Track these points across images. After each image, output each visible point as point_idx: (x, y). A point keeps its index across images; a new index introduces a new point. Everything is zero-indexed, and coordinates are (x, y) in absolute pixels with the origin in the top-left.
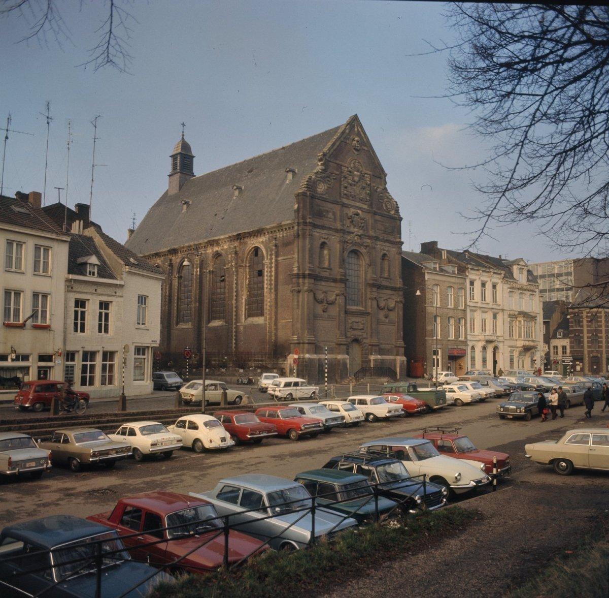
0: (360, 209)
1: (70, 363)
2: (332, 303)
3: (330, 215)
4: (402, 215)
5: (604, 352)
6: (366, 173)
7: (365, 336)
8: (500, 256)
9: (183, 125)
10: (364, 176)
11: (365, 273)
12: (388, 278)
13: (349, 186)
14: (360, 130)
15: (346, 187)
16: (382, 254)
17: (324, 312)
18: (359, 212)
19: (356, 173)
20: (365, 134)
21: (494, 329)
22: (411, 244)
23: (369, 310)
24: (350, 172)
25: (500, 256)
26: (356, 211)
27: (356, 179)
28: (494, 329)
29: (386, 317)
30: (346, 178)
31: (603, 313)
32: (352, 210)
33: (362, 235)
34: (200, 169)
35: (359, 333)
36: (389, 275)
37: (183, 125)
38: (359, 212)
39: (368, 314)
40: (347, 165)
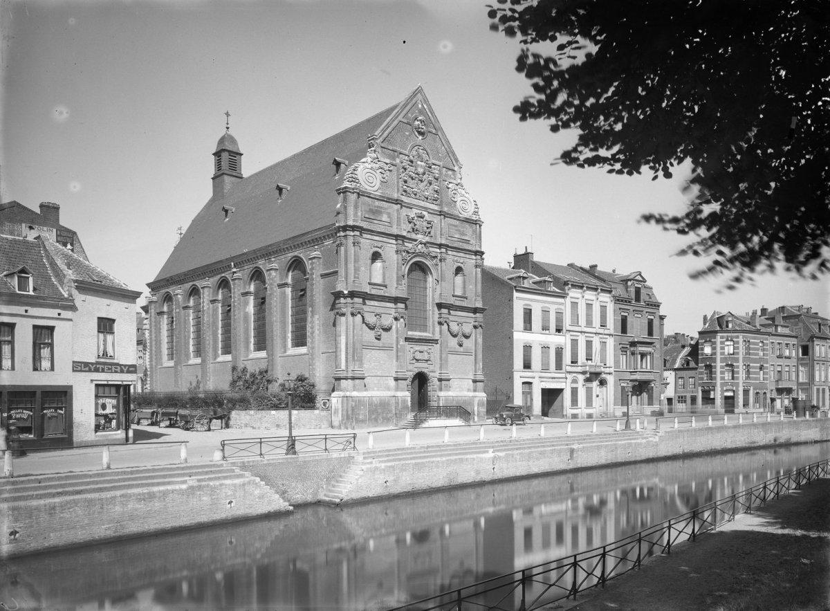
0: (426, 209)
1: (84, 408)
2: (387, 330)
3: (385, 218)
4: (624, 271)
5: (741, 385)
6: (434, 164)
7: (431, 368)
8: (614, 271)
9: (227, 114)
10: (430, 167)
11: (433, 291)
12: (464, 297)
13: (410, 180)
14: (425, 107)
15: (406, 182)
16: (455, 267)
17: (376, 338)
18: (425, 213)
19: (419, 163)
20: (432, 113)
21: (105, 341)
22: (498, 258)
23: (437, 336)
24: (412, 162)
25: (614, 271)
26: (420, 212)
27: (421, 170)
28: (105, 341)
29: (461, 345)
30: (405, 169)
31: (741, 337)
32: (415, 211)
33: (428, 243)
34: (249, 167)
35: (425, 365)
36: (465, 292)
37: (227, 114)
38: (425, 213)
39: (436, 341)
40: (407, 152)
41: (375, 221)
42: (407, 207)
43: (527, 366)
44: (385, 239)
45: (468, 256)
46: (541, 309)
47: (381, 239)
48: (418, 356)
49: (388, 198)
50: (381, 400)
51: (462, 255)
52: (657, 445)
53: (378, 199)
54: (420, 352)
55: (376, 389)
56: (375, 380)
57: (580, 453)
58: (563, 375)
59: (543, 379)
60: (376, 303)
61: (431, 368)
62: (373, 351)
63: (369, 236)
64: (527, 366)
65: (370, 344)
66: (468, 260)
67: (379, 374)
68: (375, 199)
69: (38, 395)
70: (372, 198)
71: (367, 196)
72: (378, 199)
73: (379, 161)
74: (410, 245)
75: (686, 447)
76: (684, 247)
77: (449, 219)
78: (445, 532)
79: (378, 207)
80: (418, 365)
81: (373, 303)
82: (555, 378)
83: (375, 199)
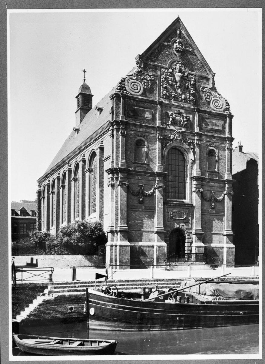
9: (85, 71)
37: (85, 71)
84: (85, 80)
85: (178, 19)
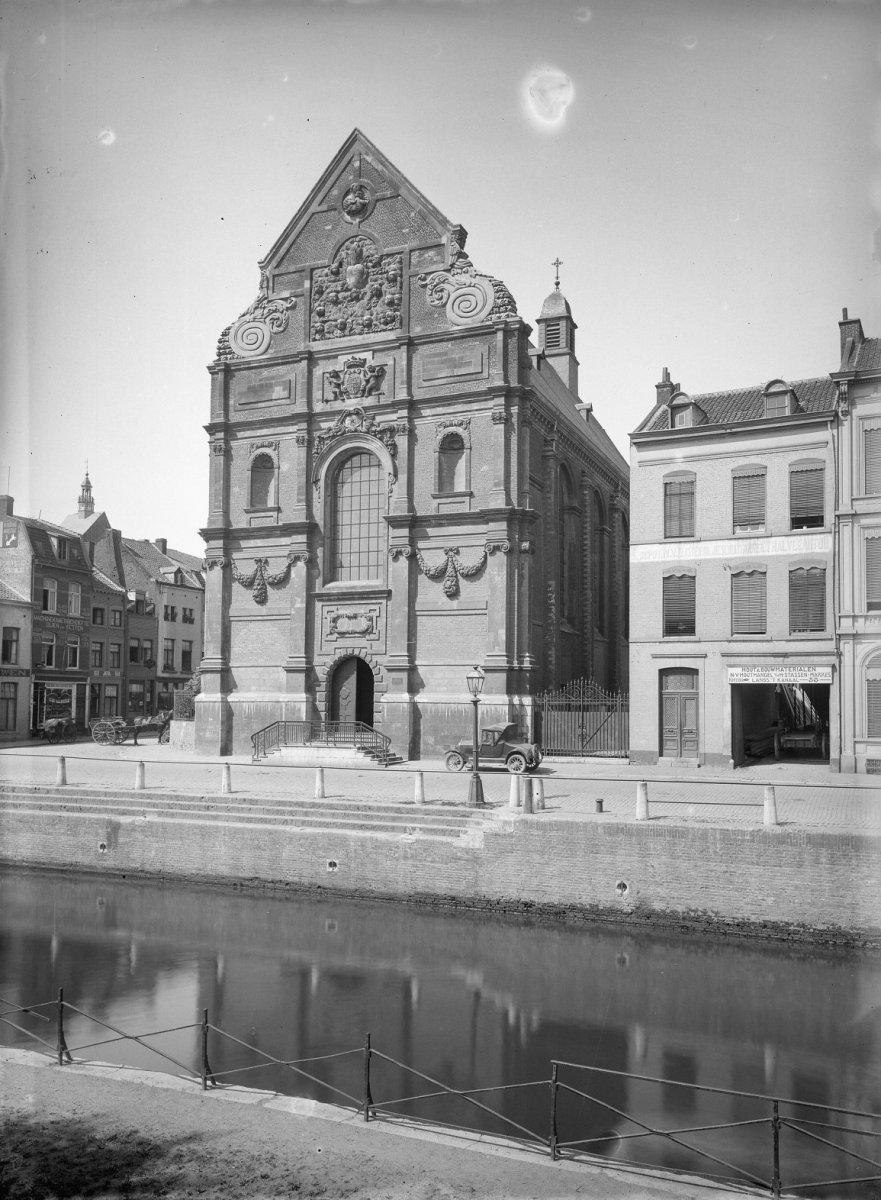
0: (365, 347)
3: (279, 392)
7: (378, 646)
14: (369, 159)
16: (440, 437)
26: (349, 357)
32: (343, 359)
35: (363, 642)
41: (260, 405)
42: (328, 358)
43: (679, 624)
44: (279, 430)
45: (475, 406)
46: (730, 476)
47: (271, 431)
48: (344, 625)
49: (284, 357)
50: (258, 710)
51: (459, 408)
52: (474, 858)
53: (266, 366)
54: (349, 618)
55: (253, 688)
56: (252, 673)
57: (139, 836)
58: (830, 646)
59: (733, 660)
60: (259, 542)
61: (378, 646)
62: (251, 625)
63: (248, 434)
64: (679, 624)
65: (243, 613)
66: (477, 414)
67: (261, 662)
68: (261, 367)
69: (870, 601)
70: (252, 368)
71: (245, 369)
72: (266, 366)
73: (269, 302)
74: (332, 424)
75: (650, 891)
76: (94, 493)
77: (425, 347)
78: (411, 996)
79: (267, 378)
80: (342, 642)
81: (252, 543)
82: (785, 655)
83: (261, 367)
84: (557, 284)
85: (356, 132)
